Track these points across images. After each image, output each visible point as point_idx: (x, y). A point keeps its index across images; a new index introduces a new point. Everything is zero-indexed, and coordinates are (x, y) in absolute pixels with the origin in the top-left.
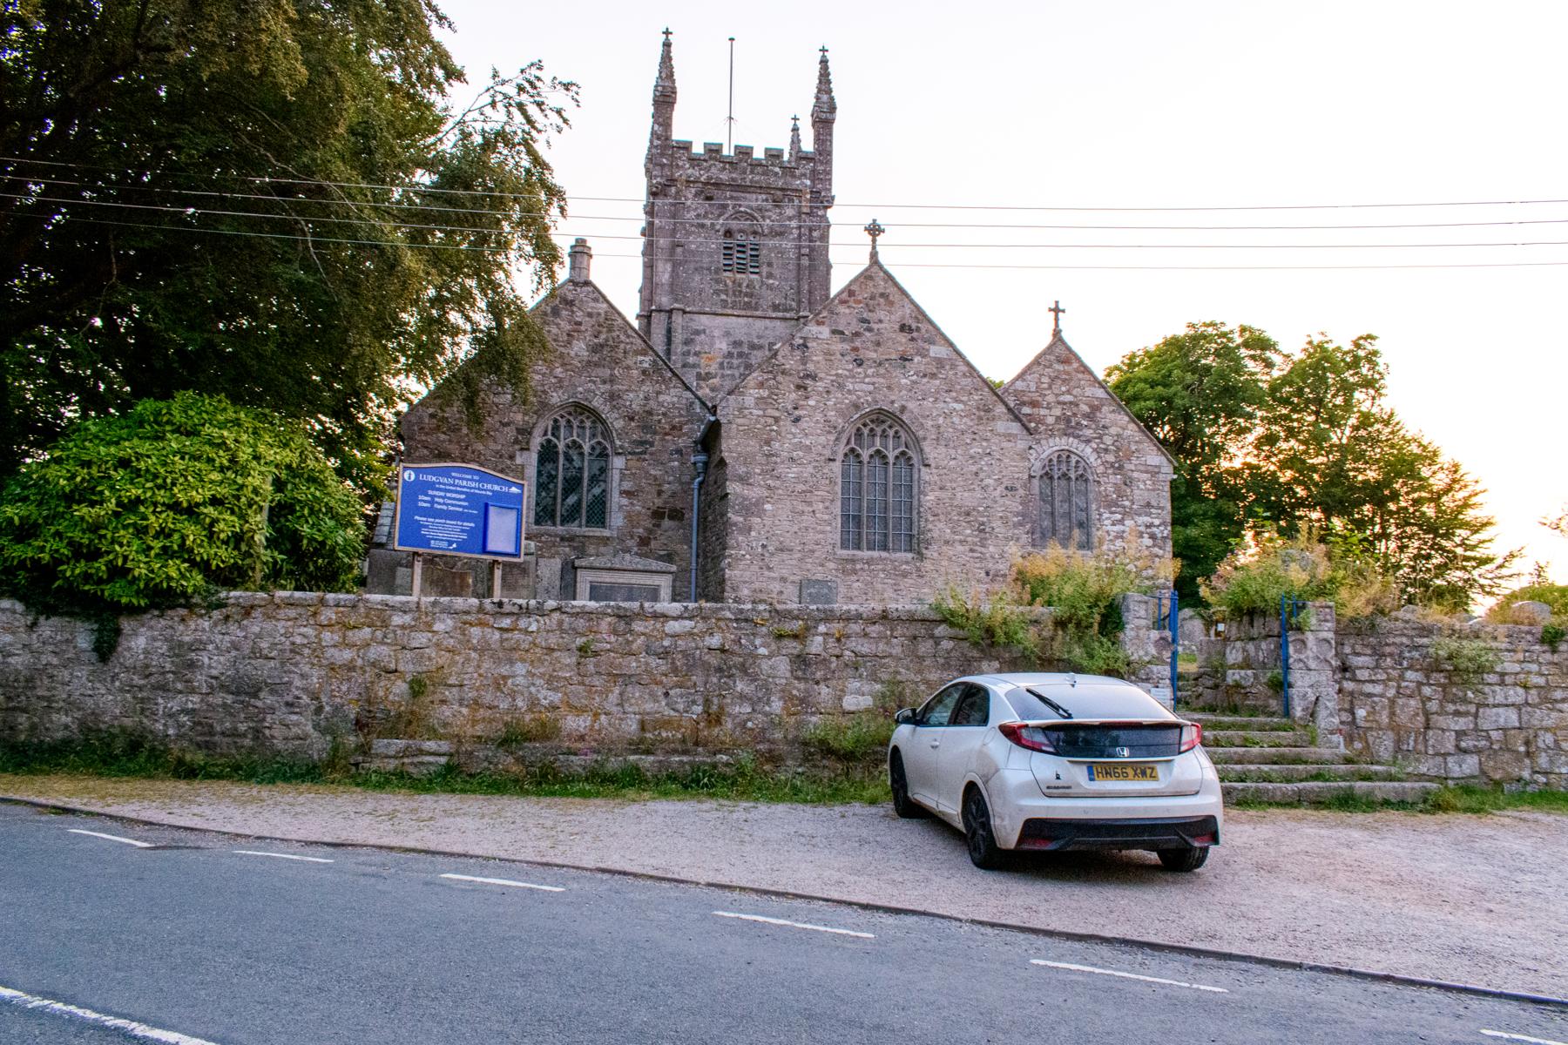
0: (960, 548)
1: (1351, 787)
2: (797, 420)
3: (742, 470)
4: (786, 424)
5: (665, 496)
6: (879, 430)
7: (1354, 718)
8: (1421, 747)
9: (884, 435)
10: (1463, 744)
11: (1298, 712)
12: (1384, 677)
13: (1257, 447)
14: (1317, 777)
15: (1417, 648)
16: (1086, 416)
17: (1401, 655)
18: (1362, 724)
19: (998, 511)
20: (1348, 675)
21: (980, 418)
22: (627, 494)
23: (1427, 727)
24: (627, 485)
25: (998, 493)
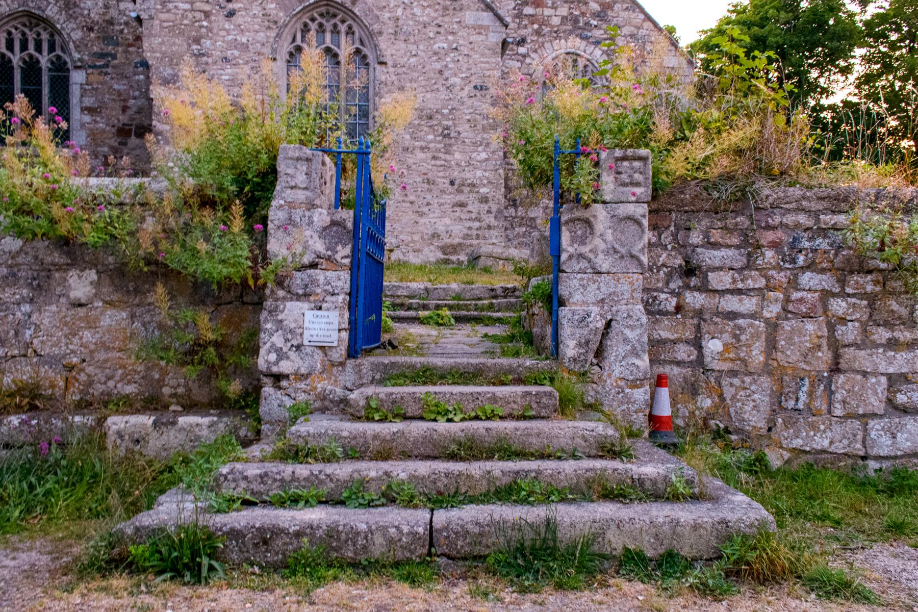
0: (420, 155)
1: (550, 525)
2: (231, 14)
3: (168, 72)
4: (218, 19)
5: (130, 112)
6: (328, 26)
7: (701, 355)
8: (820, 404)
9: (335, 31)
10: (901, 398)
11: (570, 349)
12: (762, 283)
13: (858, 87)
14: (507, 493)
15: (823, 232)
16: (596, 15)
17: (794, 245)
18: (716, 365)
19: (465, 113)
20: (694, 281)
21: (446, 8)
22: (90, 110)
23: (836, 369)
24: (89, 101)
25: (465, 93)
